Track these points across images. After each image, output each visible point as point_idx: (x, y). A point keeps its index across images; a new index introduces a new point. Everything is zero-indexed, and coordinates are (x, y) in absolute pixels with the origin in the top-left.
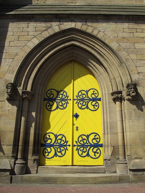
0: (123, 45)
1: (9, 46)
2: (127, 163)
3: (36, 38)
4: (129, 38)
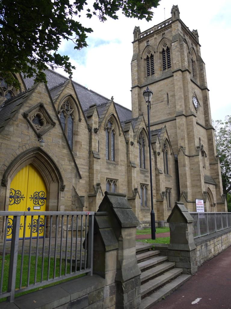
2: (57, 211)
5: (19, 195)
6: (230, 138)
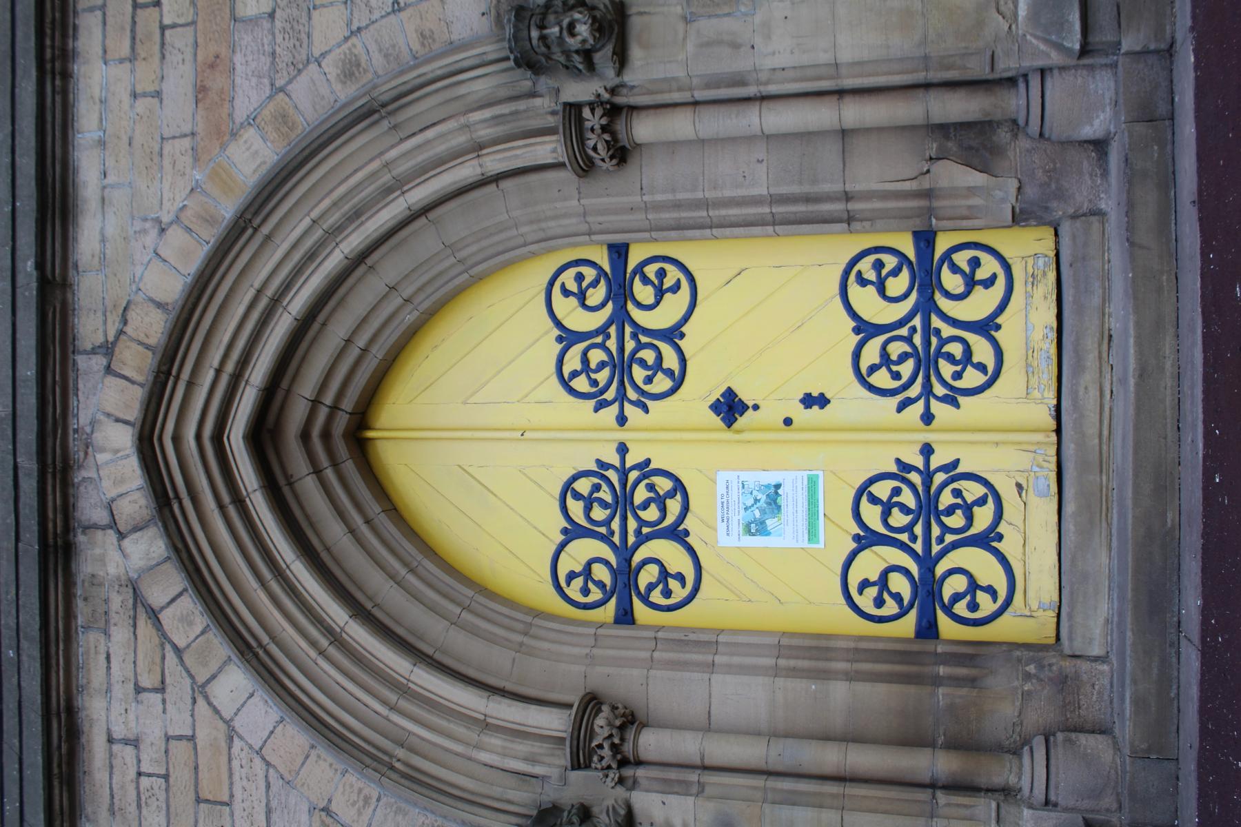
3: (208, 681)
4: (200, 58)
5: (908, 498)
6: (174, 7)
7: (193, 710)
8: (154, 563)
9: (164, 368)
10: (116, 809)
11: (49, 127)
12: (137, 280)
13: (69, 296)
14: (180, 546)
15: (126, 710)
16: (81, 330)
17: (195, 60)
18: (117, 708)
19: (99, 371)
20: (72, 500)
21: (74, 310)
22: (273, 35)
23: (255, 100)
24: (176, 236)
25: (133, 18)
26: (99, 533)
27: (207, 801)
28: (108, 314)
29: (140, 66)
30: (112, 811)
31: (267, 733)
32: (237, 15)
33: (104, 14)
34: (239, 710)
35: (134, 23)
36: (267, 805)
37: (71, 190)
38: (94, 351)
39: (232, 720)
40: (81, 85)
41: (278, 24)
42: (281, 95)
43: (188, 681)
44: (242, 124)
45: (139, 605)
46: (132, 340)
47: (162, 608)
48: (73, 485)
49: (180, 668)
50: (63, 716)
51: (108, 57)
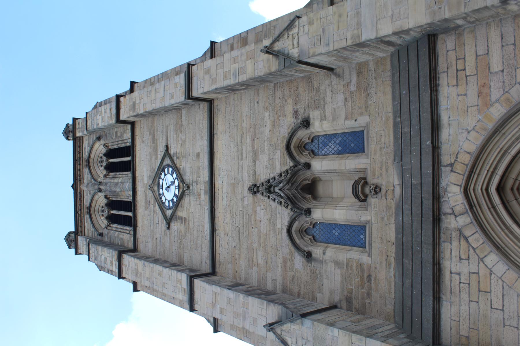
0: (495, 94)
1: (503, 310)
3: (484, 257)
4: (479, 84)
7: (478, 265)
8: (467, 224)
9: (471, 170)
10: (452, 292)
11: (433, 105)
12: (461, 146)
13: (439, 151)
14: (477, 219)
15: (456, 265)
16: (443, 160)
17: (478, 85)
18: (453, 264)
19: (449, 171)
20: (440, 206)
21: (441, 154)
22: (503, 76)
23: (498, 96)
24: (473, 133)
25: (457, 74)
26: (449, 216)
27: (482, 291)
28: (451, 155)
29: (459, 87)
30: (451, 292)
31: (503, 273)
32: (491, 72)
33: (447, 74)
34: (494, 266)
35: (457, 75)
36: (503, 293)
37: (439, 122)
38: (447, 166)
39: (491, 268)
40: (441, 93)
41: (505, 73)
42: (507, 94)
43: (477, 257)
44: (494, 102)
45: (461, 235)
46: (460, 162)
47: (469, 237)
48: (441, 202)
49: (474, 253)
50: (437, 265)
51: (449, 85)
